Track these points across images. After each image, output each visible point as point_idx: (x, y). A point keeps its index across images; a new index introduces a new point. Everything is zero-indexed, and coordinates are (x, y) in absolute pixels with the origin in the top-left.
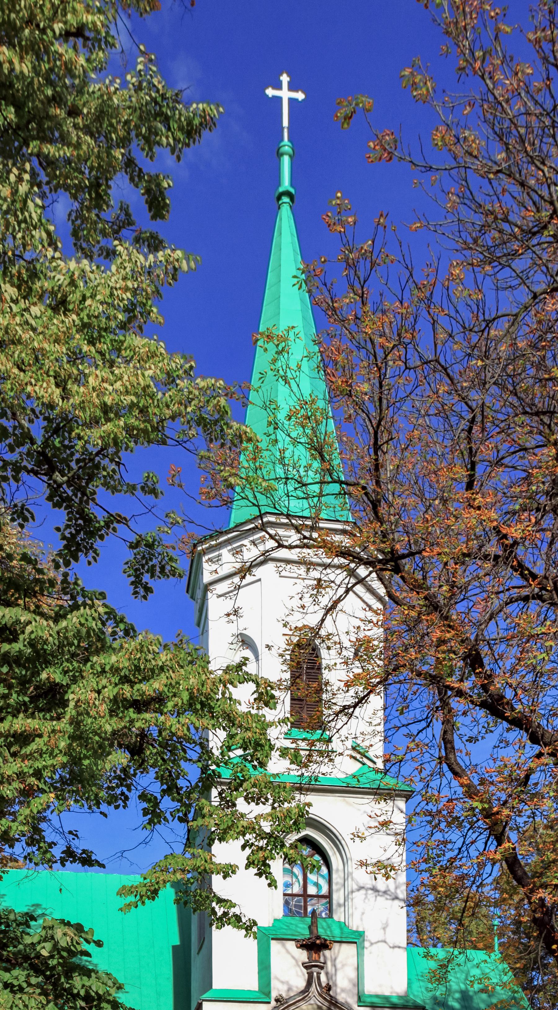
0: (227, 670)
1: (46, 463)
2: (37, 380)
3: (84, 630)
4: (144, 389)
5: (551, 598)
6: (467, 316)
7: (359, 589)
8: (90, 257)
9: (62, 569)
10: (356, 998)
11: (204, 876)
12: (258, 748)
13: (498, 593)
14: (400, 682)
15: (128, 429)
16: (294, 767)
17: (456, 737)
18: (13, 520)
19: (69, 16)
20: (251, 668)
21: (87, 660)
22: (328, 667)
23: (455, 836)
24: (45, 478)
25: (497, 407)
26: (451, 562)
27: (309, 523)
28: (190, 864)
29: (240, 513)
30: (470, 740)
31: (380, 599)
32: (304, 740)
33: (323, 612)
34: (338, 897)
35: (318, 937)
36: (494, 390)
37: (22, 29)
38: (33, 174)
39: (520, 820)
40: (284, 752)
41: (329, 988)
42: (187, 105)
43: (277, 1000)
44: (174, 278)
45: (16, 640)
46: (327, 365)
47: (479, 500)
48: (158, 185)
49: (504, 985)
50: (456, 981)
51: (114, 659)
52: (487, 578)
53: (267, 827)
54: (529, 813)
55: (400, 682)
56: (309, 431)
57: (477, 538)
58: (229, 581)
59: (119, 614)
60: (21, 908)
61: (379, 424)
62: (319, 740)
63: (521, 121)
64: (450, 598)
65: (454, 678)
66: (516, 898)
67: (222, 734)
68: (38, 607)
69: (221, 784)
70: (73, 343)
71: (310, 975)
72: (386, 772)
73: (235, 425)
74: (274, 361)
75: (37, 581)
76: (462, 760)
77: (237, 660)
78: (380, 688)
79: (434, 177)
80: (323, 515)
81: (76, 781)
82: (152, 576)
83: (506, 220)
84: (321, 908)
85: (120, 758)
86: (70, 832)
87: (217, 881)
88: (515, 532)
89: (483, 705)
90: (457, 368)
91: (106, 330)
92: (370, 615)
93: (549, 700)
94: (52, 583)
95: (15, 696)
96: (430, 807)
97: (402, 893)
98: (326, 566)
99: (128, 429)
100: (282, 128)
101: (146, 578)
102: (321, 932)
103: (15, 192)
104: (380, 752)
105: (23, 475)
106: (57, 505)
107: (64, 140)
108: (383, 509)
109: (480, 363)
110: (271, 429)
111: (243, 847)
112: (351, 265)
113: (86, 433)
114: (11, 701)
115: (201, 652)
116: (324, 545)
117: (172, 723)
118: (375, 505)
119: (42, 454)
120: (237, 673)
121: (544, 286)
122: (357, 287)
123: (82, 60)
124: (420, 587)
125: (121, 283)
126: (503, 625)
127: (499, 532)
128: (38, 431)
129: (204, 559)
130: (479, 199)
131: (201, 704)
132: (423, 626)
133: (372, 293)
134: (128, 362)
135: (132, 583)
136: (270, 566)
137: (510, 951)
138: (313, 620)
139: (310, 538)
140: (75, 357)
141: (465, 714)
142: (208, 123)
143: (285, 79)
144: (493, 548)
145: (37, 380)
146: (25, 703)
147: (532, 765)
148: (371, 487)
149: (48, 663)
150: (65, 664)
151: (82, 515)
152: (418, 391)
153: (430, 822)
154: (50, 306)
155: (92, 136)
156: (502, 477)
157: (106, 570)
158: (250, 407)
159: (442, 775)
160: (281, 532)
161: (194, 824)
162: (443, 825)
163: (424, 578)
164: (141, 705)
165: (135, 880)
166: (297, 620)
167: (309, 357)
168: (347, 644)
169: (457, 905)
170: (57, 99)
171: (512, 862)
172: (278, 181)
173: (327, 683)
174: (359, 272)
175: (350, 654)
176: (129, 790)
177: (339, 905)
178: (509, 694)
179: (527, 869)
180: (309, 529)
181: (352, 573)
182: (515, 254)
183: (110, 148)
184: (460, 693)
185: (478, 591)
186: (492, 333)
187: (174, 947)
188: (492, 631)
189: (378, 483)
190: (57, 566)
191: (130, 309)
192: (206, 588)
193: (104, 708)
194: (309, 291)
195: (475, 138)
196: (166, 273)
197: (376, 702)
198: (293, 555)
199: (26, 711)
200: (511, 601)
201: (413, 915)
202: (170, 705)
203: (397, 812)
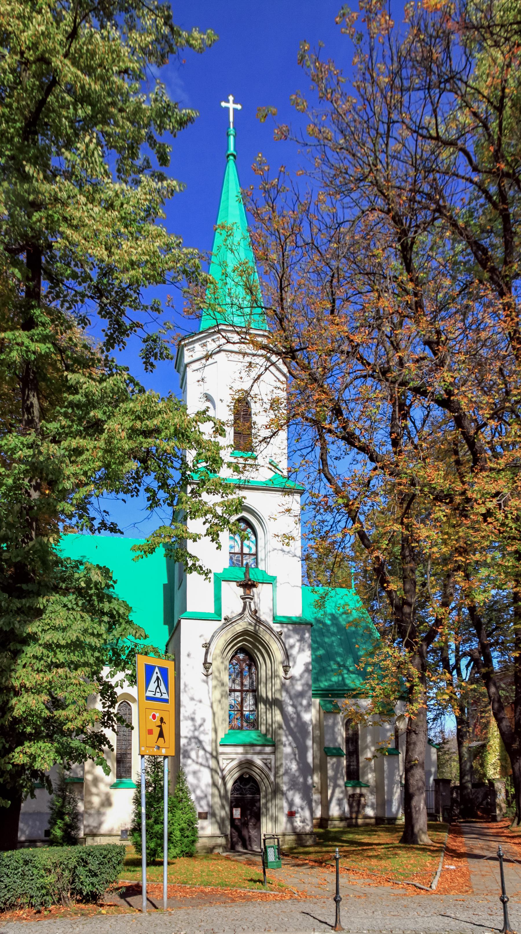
0: (198, 414)
1: (99, 292)
2: (95, 247)
3: (116, 388)
4: (154, 253)
5: (379, 377)
6: (328, 221)
7: (272, 368)
8: (126, 182)
9: (105, 353)
10: (272, 618)
11: (182, 540)
12: (215, 462)
13: (349, 373)
14: (297, 424)
15: (145, 275)
16: (236, 473)
17: (328, 458)
18: (79, 324)
19: (121, 64)
20: (211, 413)
21: (116, 406)
22: (255, 414)
23: (328, 517)
24: (98, 301)
25: (346, 269)
26: (323, 355)
27: (244, 330)
28: (175, 532)
29: (206, 323)
30: (336, 458)
31: (284, 375)
32: (242, 457)
33: (252, 381)
34: (261, 555)
35: (250, 580)
36: (343, 260)
37: (96, 69)
38: (97, 138)
39: (366, 508)
40: (229, 465)
41: (256, 612)
42: (180, 110)
43: (225, 619)
44: (172, 195)
45: (77, 393)
46: (254, 243)
47: (337, 320)
48: (164, 150)
49: (357, 609)
50: (330, 608)
51: (132, 405)
52: (343, 365)
53: (219, 511)
54: (370, 504)
55: (297, 424)
56: (245, 279)
57: (337, 341)
58: (199, 362)
59: (137, 380)
60: (75, 557)
61: (282, 276)
62: (249, 458)
63: (352, 124)
64: (323, 375)
65: (327, 422)
66: (364, 556)
67: (194, 453)
68: (90, 374)
69: (194, 483)
70: (116, 228)
71: (245, 604)
72: (289, 478)
73: (204, 274)
74: (226, 240)
75: (92, 359)
76: (332, 471)
77: (203, 408)
78: (285, 427)
79: (308, 149)
80: (252, 326)
81: (110, 479)
82: (155, 359)
83: (346, 173)
84: (252, 562)
85: (133, 465)
86: (105, 511)
87: (189, 542)
88: (357, 339)
89: (343, 438)
90: (324, 247)
91: (134, 221)
92: (279, 384)
93: (379, 437)
94: (99, 360)
95: (75, 426)
96: (314, 500)
97: (299, 553)
98: (254, 355)
99: (145, 275)
100: (229, 123)
101: (152, 359)
102: (251, 577)
103: (87, 146)
104: (286, 466)
105: (86, 299)
106: (104, 317)
107: (116, 124)
108: (286, 323)
109: (335, 245)
110: (224, 277)
111: (204, 523)
112: (267, 191)
113: (121, 276)
114: (73, 429)
115: (182, 403)
116: (252, 342)
117: (166, 446)
118: (281, 321)
119: (96, 287)
120: (203, 416)
121: (367, 208)
122: (270, 203)
123: (126, 86)
124: (307, 368)
125: (143, 197)
126: (353, 392)
127: (349, 338)
128: (95, 275)
129: (185, 349)
130: (332, 161)
131: (181, 434)
132: (308, 392)
133: (278, 205)
134: (145, 238)
135: (144, 363)
136: (223, 354)
137: (361, 589)
138: (246, 386)
139: (246, 339)
140: (117, 234)
141: (333, 443)
142: (191, 119)
143: (231, 98)
144: (346, 347)
145: (95, 247)
146: (80, 431)
147: (372, 475)
148: (279, 310)
149: (95, 407)
150: (105, 408)
151: (118, 322)
152: (303, 259)
153: (314, 509)
154: (104, 207)
155: (130, 122)
156: (350, 308)
157: (129, 354)
158: (212, 265)
159: (320, 480)
160: (229, 335)
161: (177, 507)
162: (322, 511)
163: (309, 363)
164: (147, 433)
165: (142, 542)
166: (238, 386)
167: (244, 238)
168: (265, 400)
169: (331, 560)
170: (113, 104)
171: (362, 536)
172: (228, 148)
173: (255, 423)
174: (271, 196)
175: (268, 406)
176: (140, 486)
177: (262, 560)
178: (357, 432)
179: (370, 538)
180: (244, 333)
181: (268, 359)
182: (351, 190)
183: (139, 128)
184: (330, 431)
185: (338, 372)
186: (342, 229)
187: (164, 585)
188: (347, 395)
189: (283, 309)
190: (103, 352)
191: (147, 211)
192: (186, 366)
193: (124, 434)
194: (245, 204)
195: (330, 132)
196: (168, 192)
197: (283, 435)
198: (235, 348)
199: (80, 436)
200: (357, 378)
201: (305, 567)
202: (163, 434)
203: (295, 502)
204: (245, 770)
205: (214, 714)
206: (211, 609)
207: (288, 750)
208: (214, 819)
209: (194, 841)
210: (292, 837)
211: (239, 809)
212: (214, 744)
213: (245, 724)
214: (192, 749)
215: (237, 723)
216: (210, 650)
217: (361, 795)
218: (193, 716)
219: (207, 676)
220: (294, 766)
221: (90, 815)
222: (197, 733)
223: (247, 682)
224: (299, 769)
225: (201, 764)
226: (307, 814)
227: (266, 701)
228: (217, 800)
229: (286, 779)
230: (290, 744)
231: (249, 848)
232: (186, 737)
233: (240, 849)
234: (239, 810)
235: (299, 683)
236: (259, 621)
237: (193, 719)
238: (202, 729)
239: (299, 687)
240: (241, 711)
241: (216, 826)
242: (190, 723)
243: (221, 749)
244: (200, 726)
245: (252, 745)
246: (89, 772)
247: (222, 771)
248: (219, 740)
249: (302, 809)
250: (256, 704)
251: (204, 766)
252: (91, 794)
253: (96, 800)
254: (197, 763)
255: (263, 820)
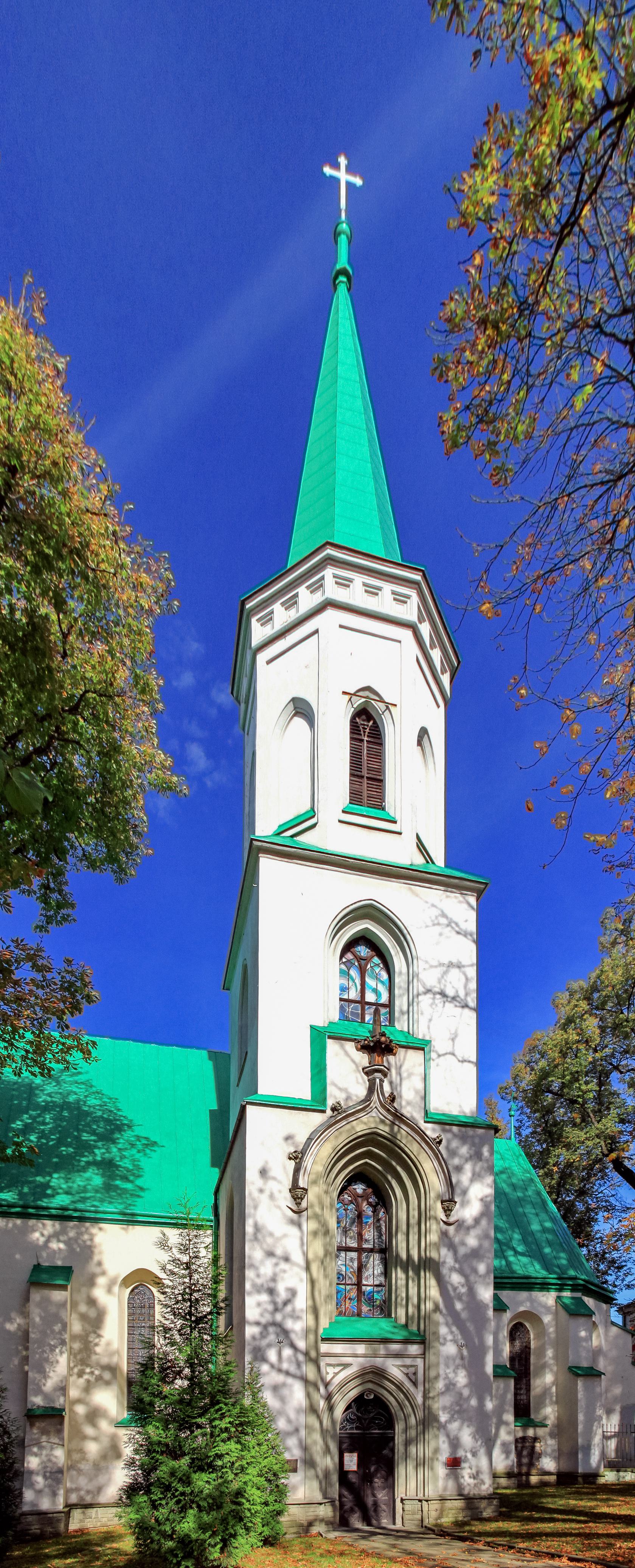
34: (401, 1003)
41: (393, 1099)
43: (334, 1109)
143: (343, 161)
148: (537, 127)
187: (210, 1111)
204: (370, 1386)
205: (312, 1282)
206: (303, 1092)
207: (450, 1349)
208: (311, 1472)
209: (279, 1513)
210: (460, 1504)
211: (355, 1455)
212: (312, 1337)
213: (365, 1308)
214: (269, 1346)
215: (351, 1305)
216: (304, 1164)
217: (535, 1439)
218: (271, 1285)
219: (298, 1212)
220: (461, 1379)
221: (79, 1471)
222: (278, 1317)
223: (369, 1234)
224: (469, 1385)
225: (287, 1373)
226: (484, 1462)
227: (407, 1264)
228: (317, 1437)
229: (446, 1400)
230: (455, 1341)
231: (374, 1522)
232: (258, 1323)
233: (357, 1522)
234: (355, 1456)
235: (473, 1233)
236: (398, 1117)
237: (271, 1292)
238: (289, 1308)
239: (472, 1241)
240: (359, 1284)
241: (315, 1484)
242: (264, 1297)
243: (324, 1348)
244: (285, 1303)
245: (385, 1341)
246: (79, 1401)
247: (327, 1385)
248: (321, 1331)
249: (474, 1454)
250: (386, 1273)
251: (294, 1376)
252: (85, 1438)
253: (92, 1448)
254: (280, 1370)
255: (401, 1472)
